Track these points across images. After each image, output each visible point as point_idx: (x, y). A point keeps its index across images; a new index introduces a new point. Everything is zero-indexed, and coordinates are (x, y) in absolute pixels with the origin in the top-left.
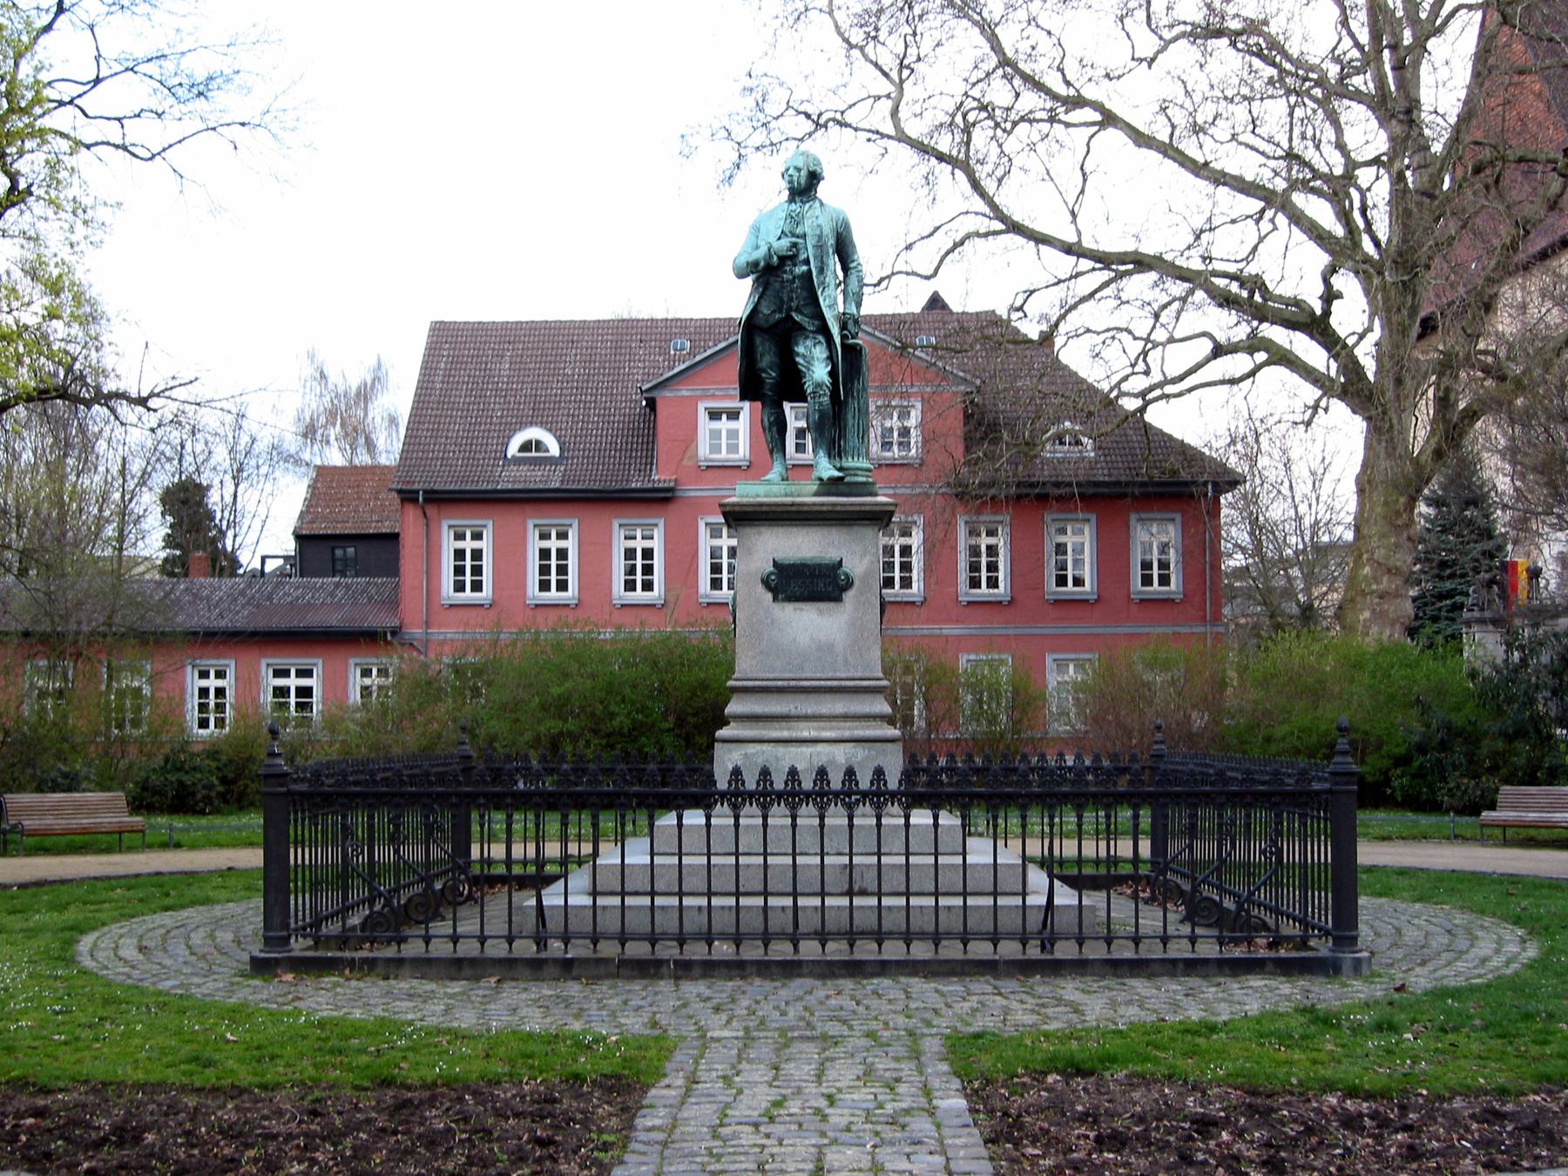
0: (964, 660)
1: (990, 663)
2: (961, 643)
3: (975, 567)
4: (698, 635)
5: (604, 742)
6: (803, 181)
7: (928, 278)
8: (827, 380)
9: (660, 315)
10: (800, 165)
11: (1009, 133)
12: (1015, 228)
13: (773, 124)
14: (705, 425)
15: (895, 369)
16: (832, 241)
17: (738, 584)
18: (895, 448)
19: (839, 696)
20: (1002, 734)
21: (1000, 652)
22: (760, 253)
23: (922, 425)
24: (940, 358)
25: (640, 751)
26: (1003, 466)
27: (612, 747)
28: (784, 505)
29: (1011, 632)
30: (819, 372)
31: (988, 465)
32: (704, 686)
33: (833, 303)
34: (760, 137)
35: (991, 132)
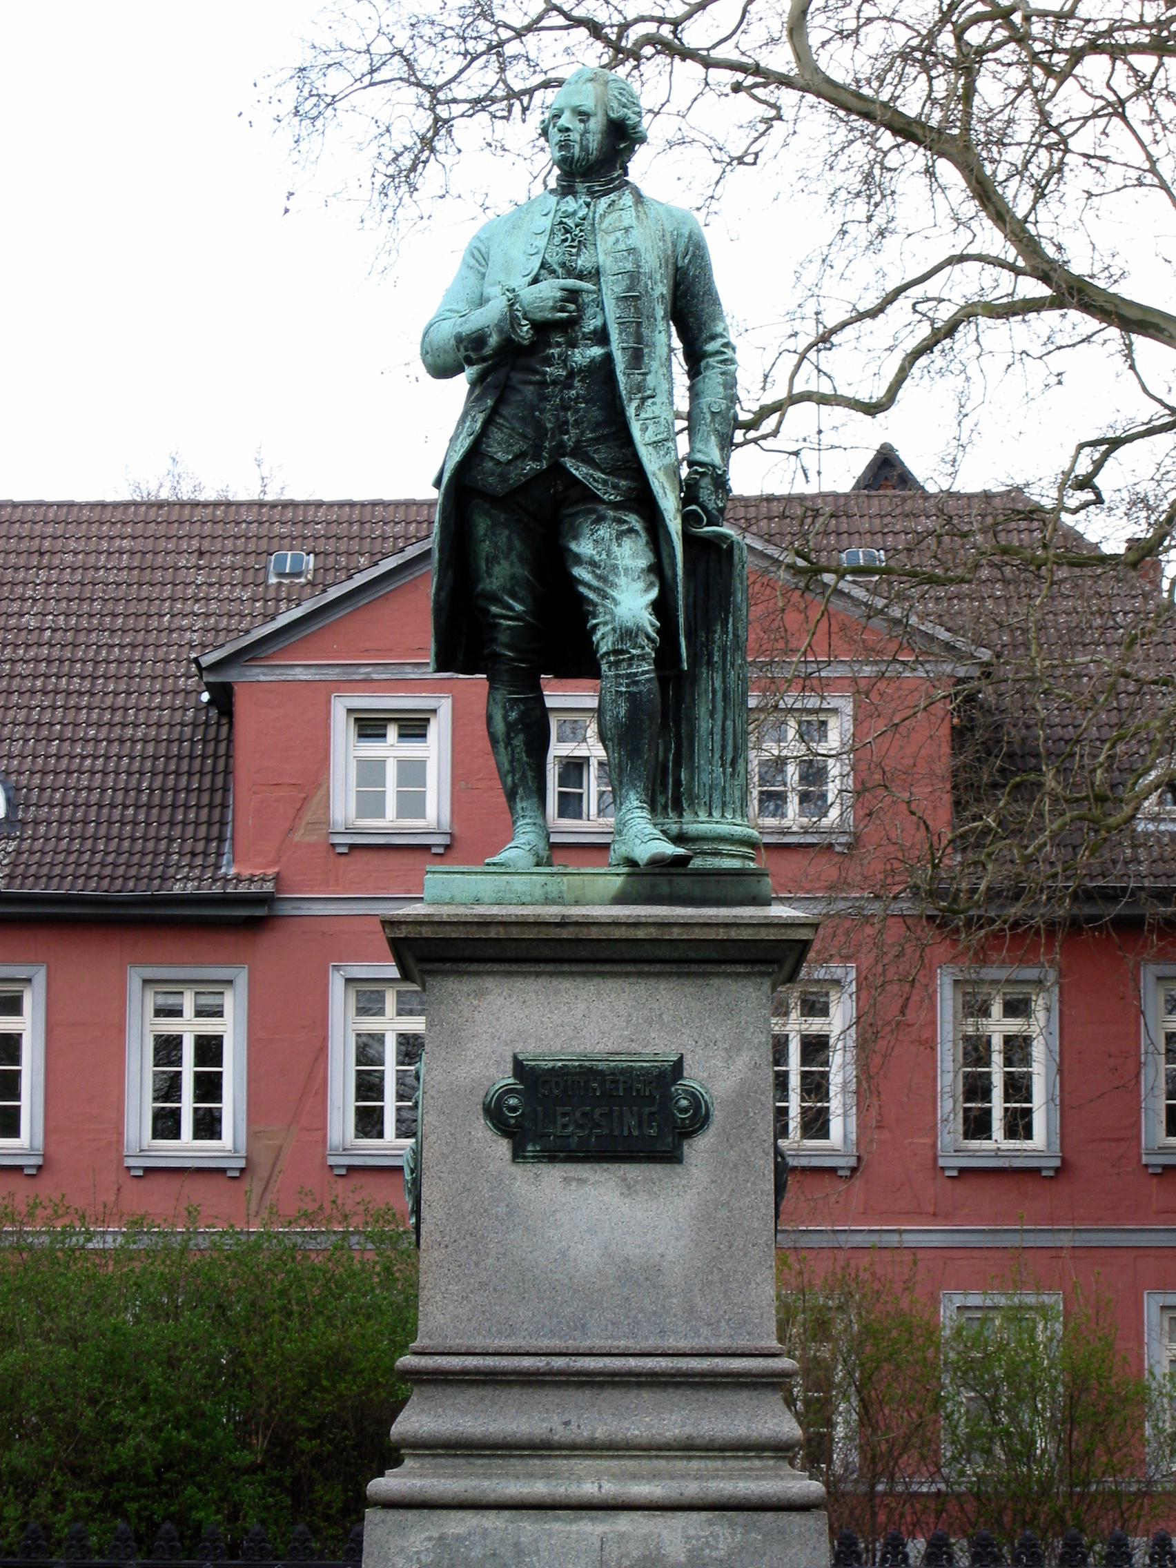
0: (949, 1310)
1: (1015, 1315)
2: (949, 1265)
3: (977, 1089)
4: (325, 1243)
5: (96, 1497)
6: (594, 142)
7: (872, 409)
8: (647, 620)
9: (245, 491)
10: (588, 104)
11: (1062, 76)
12: (1074, 293)
13: (511, 49)
14: (346, 750)
15: (792, 618)
16: (662, 289)
17: (429, 1120)
18: (793, 805)
19: (675, 1396)
20: (1046, 1486)
21: (1039, 1289)
22: (490, 315)
23: (856, 748)
24: (901, 597)
25: (179, 1519)
26: (1043, 850)
27: (116, 1509)
28: (539, 924)
29: (1065, 1240)
30: (630, 602)
31: (1009, 848)
32: (338, 1364)
33: (663, 438)
34: (481, 79)
35: (1016, 76)
